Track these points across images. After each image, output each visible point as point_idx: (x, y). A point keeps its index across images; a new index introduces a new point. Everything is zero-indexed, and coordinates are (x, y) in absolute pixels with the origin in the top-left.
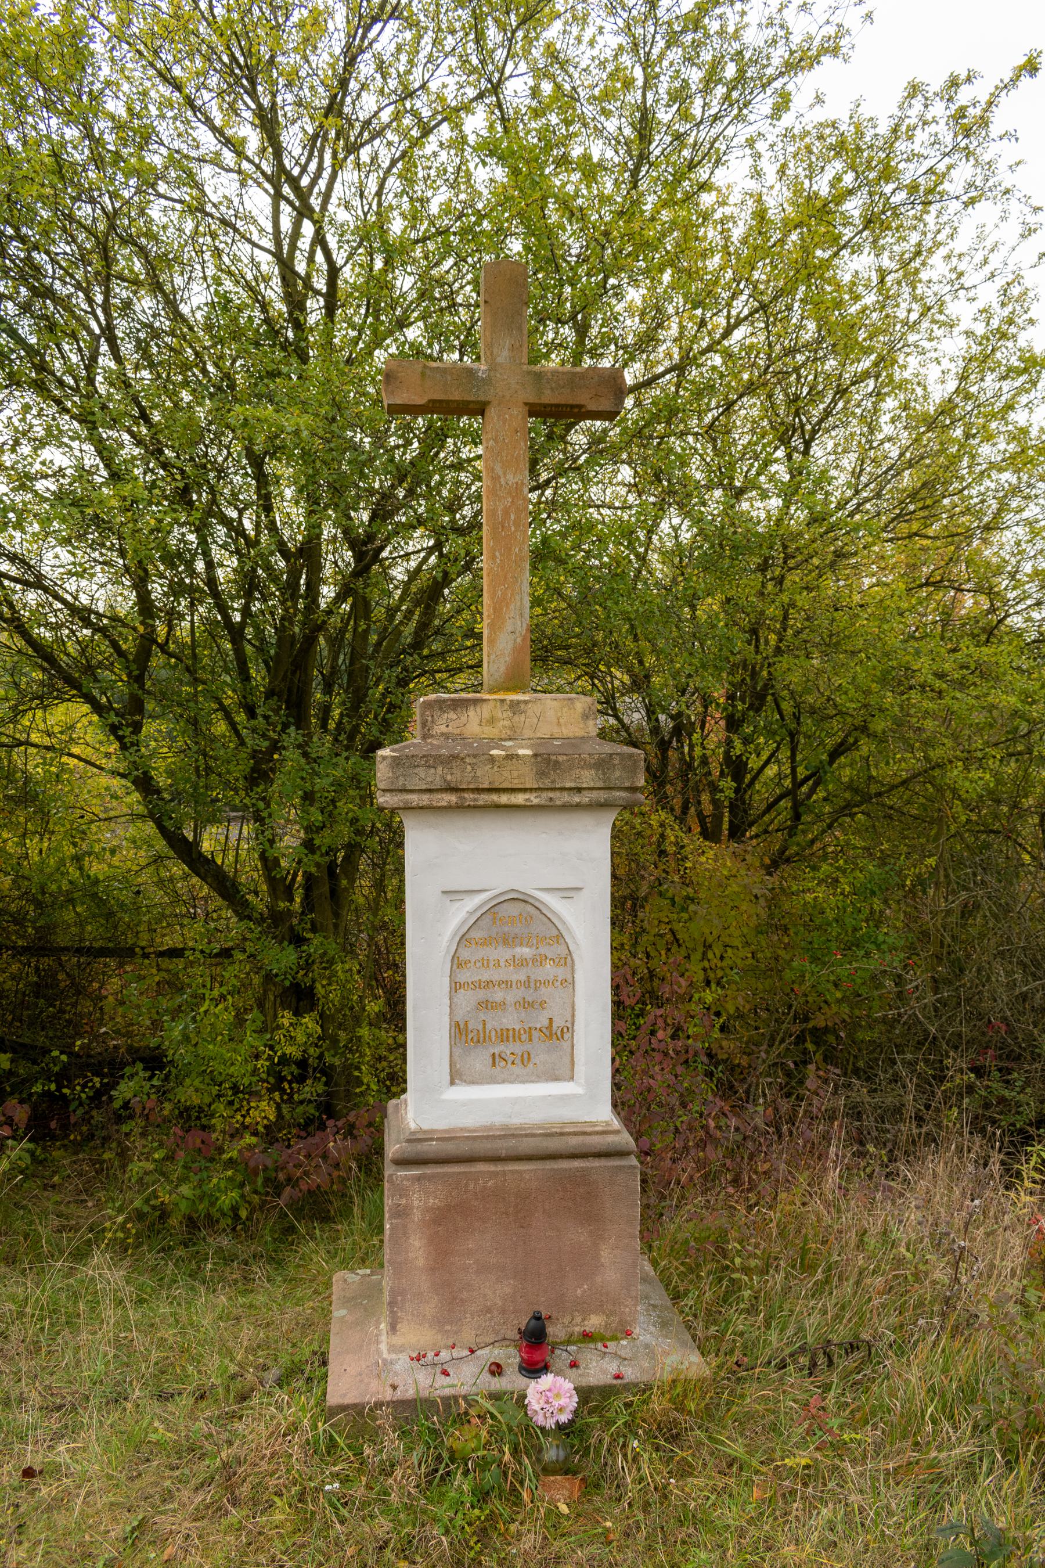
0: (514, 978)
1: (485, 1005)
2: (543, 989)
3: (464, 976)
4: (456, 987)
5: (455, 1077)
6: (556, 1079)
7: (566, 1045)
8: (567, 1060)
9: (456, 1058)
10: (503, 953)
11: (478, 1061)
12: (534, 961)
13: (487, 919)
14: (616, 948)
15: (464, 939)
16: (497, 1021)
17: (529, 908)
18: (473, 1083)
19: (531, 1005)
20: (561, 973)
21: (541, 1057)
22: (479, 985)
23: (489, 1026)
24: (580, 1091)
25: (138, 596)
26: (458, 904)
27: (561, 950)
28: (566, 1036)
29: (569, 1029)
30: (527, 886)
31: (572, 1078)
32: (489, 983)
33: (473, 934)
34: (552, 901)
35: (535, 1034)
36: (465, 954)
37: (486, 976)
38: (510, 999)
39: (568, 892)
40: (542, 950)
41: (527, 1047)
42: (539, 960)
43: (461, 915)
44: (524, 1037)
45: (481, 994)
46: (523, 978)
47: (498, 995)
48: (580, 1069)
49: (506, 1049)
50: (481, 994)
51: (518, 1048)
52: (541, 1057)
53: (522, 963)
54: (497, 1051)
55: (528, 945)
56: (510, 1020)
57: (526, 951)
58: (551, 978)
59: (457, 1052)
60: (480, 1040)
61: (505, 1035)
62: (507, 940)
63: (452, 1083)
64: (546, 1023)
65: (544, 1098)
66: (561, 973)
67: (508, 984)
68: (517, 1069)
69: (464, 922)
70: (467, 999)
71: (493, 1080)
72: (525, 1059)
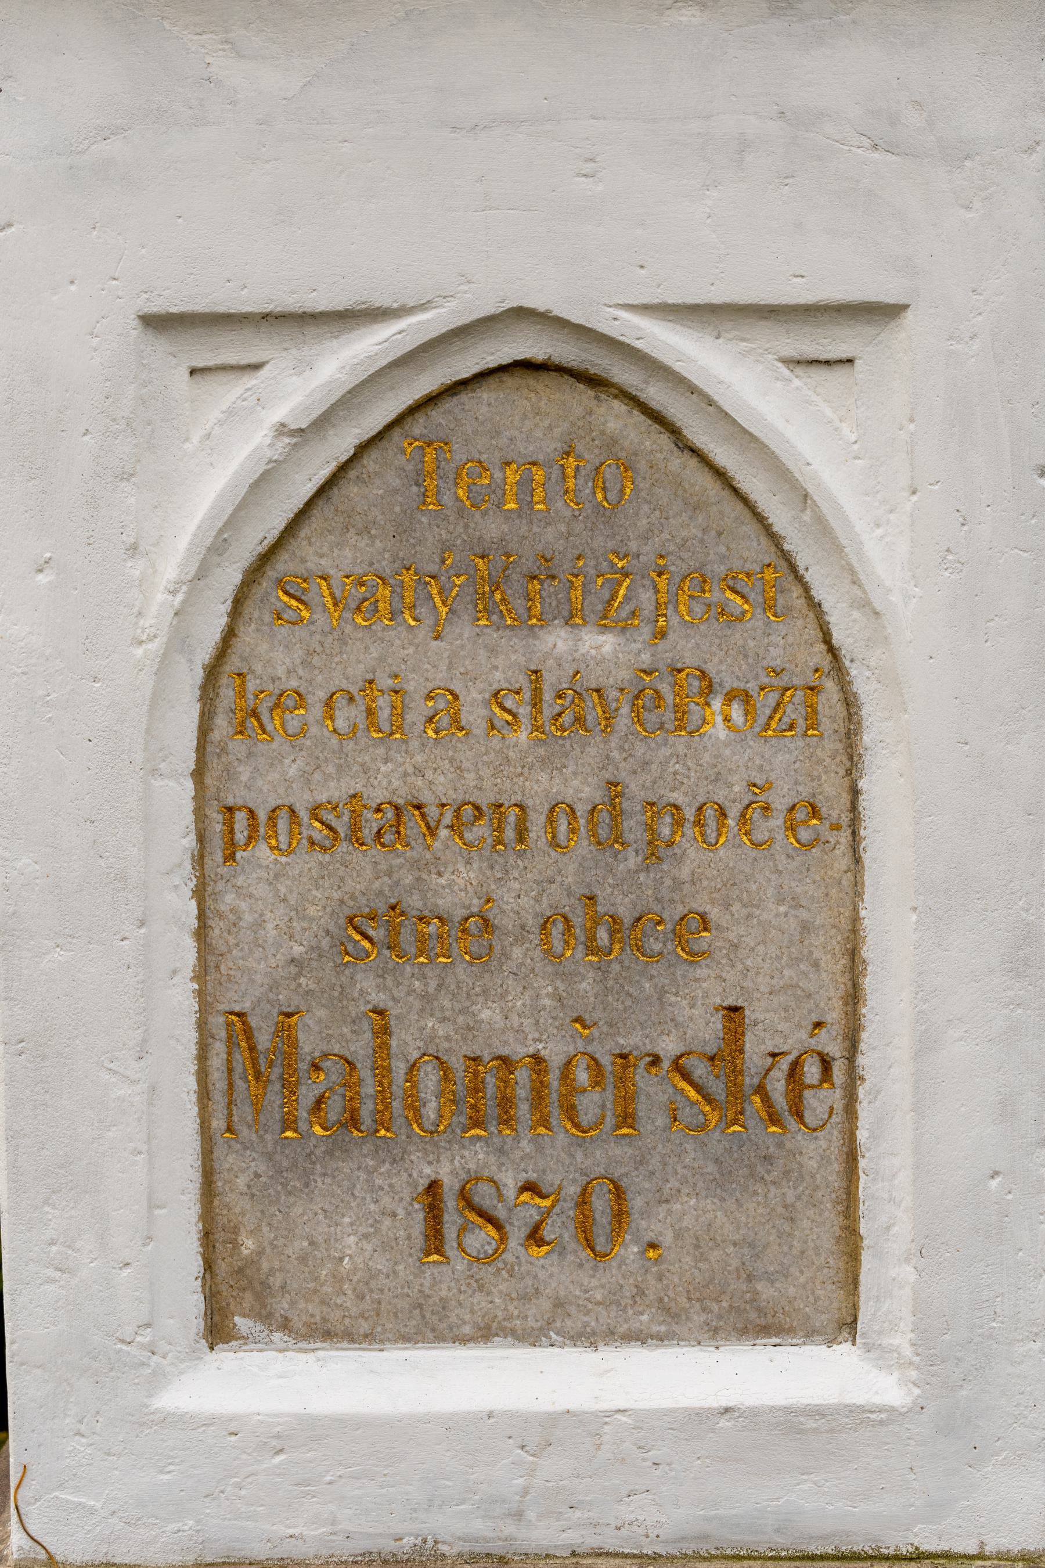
0: (539, 788)
1: (378, 930)
2: (692, 855)
3: (272, 776)
4: (225, 831)
5: (233, 1301)
6: (761, 1323)
7: (815, 1151)
8: (819, 1230)
9: (235, 1200)
10: (475, 660)
11: (352, 1221)
12: (642, 697)
13: (386, 477)
14: (773, 1409)
15: (265, 577)
16: (444, 1016)
17: (615, 418)
18: (325, 1333)
19: (630, 932)
20: (788, 767)
21: (683, 1210)
22: (343, 826)
23: (406, 1043)
24: (887, 1389)
25: (212, 1202)
26: (232, 392)
27: (790, 646)
28: (819, 1102)
29: (825, 1072)
30: (592, 276)
31: (848, 1326)
32: (403, 816)
33: (313, 553)
34: (736, 375)
35: (653, 1090)
36: (273, 656)
37: (387, 778)
38: (518, 901)
39: (828, 328)
40: (687, 647)
41: (610, 1155)
42: (664, 700)
43: (251, 445)
44: (591, 1104)
45: (364, 875)
46: (582, 789)
47: (456, 882)
48: (890, 1276)
49: (498, 1163)
50: (364, 875)
51: (561, 1160)
52: (683, 1210)
53: (572, 710)
54: (447, 1172)
55: (605, 621)
56: (519, 1013)
57: (599, 650)
58: (733, 793)
59: (241, 1170)
60: (358, 1114)
61: (489, 1094)
62: (507, 589)
63: (217, 1331)
64: (708, 1030)
65: (698, 1421)
66: (788, 767)
67: (500, 823)
68: (559, 1272)
69: (263, 483)
70: (284, 898)
71: (430, 1325)
72: (601, 1218)
